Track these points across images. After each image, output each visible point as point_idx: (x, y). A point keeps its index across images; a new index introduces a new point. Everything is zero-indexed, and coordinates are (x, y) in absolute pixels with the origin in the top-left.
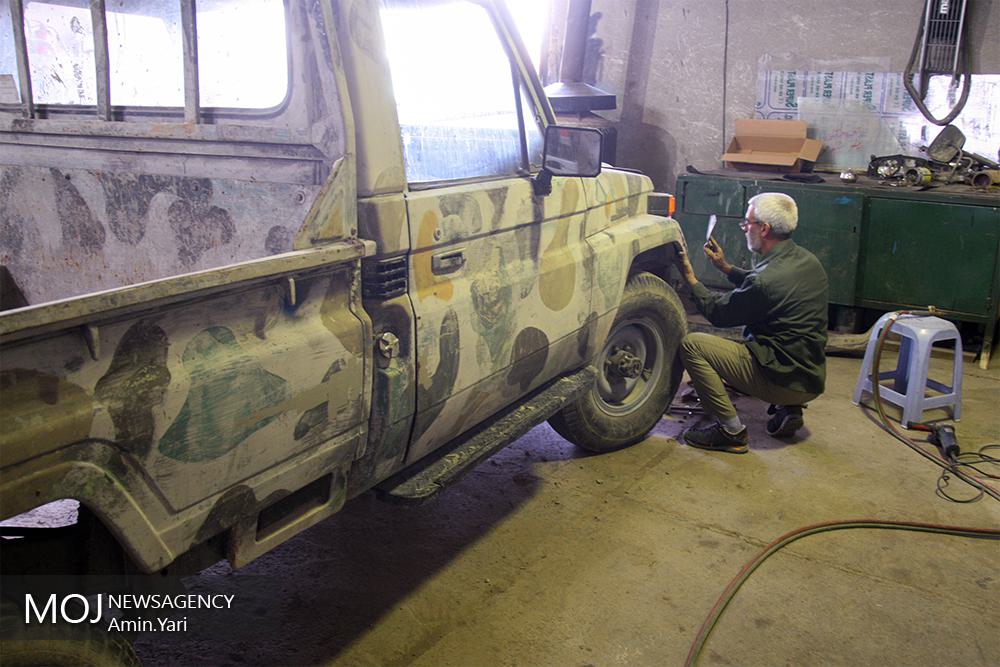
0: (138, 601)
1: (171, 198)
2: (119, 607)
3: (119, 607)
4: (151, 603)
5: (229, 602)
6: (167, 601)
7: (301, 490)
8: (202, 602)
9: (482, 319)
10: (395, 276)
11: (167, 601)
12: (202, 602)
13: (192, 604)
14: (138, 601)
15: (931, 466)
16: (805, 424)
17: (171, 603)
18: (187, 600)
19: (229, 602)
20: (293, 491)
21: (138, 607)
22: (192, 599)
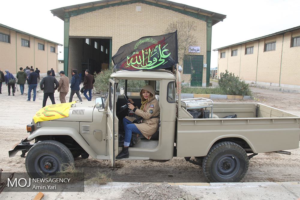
0: (41, 180)
1: (101, 136)
2: (36, 182)
3: (36, 182)
4: (45, 181)
5: (69, 181)
6: (50, 180)
7: (86, 152)
8: (61, 181)
9: (176, 117)
10: (208, 114)
11: (50, 180)
12: (61, 181)
13: (58, 181)
14: (41, 180)
15: (256, 64)
16: (247, 82)
17: (51, 181)
18: (56, 180)
19: (69, 181)
20: (122, 150)
21: (41, 182)
22: (58, 179)
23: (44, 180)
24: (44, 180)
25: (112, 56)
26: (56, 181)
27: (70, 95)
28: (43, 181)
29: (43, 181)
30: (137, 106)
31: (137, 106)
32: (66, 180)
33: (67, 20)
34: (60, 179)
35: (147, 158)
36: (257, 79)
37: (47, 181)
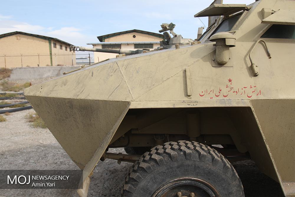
0: (41, 177)
2: (35, 179)
3: (35, 179)
4: (45, 178)
5: (68, 178)
6: (49, 178)
8: (60, 178)
11: (49, 178)
12: (60, 178)
13: (57, 179)
18: (55, 177)
19: (68, 178)
21: (41, 179)
22: (57, 177)
25: (126, 154)
26: (55, 178)
27: (89, 99)
28: (42, 178)
29: (42, 178)
30: (163, 34)
31: (163, 34)
33: (50, 41)
35: (215, 146)
36: (76, 55)
37: (46, 177)
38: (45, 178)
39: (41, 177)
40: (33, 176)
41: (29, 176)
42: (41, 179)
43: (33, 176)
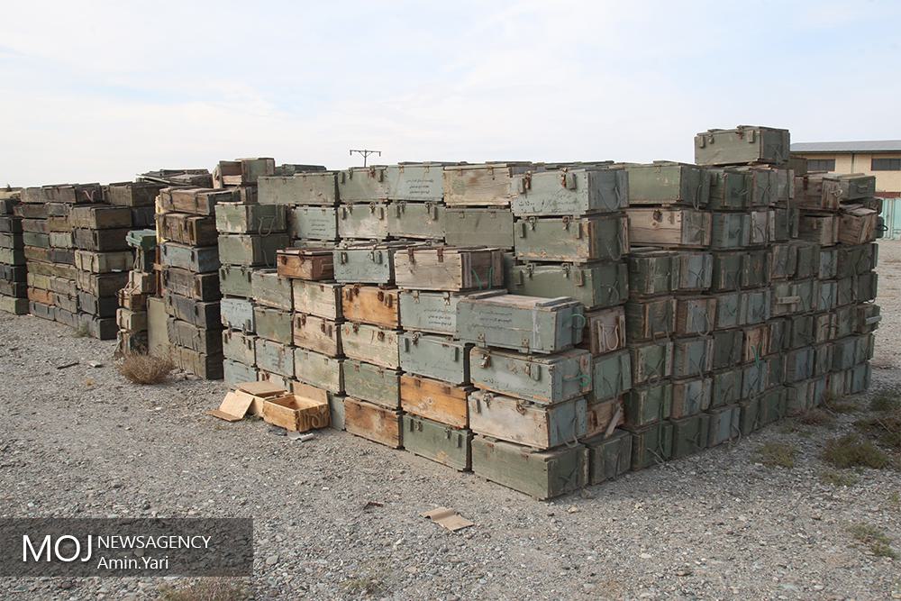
0: (124, 542)
2: (107, 547)
3: (107, 547)
4: (145, 541)
5: (206, 542)
6: (151, 542)
11: (151, 542)
13: (173, 545)
19: (206, 542)
21: (124, 547)
22: (115, 539)
23: (102, 545)
24: (102, 545)
32: (199, 542)
34: (180, 538)
38: (145, 541)
39: (124, 542)
40: (100, 537)
41: (90, 537)
42: (124, 547)
43: (100, 537)
